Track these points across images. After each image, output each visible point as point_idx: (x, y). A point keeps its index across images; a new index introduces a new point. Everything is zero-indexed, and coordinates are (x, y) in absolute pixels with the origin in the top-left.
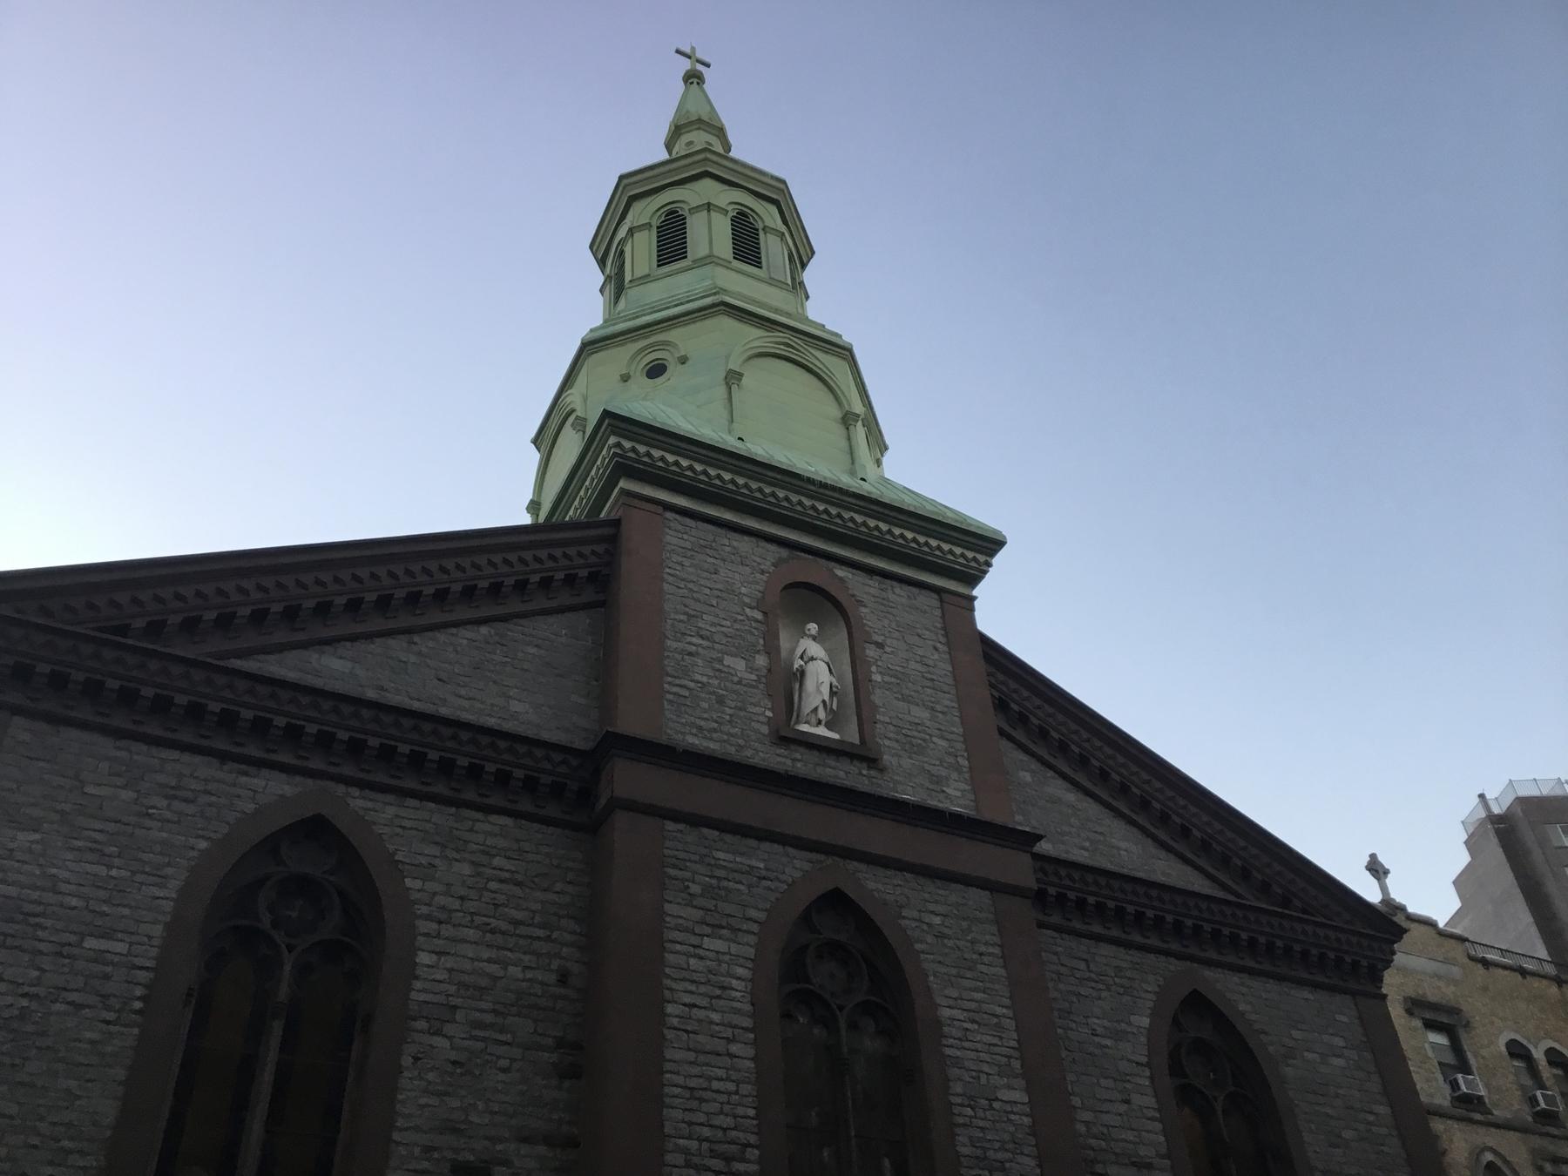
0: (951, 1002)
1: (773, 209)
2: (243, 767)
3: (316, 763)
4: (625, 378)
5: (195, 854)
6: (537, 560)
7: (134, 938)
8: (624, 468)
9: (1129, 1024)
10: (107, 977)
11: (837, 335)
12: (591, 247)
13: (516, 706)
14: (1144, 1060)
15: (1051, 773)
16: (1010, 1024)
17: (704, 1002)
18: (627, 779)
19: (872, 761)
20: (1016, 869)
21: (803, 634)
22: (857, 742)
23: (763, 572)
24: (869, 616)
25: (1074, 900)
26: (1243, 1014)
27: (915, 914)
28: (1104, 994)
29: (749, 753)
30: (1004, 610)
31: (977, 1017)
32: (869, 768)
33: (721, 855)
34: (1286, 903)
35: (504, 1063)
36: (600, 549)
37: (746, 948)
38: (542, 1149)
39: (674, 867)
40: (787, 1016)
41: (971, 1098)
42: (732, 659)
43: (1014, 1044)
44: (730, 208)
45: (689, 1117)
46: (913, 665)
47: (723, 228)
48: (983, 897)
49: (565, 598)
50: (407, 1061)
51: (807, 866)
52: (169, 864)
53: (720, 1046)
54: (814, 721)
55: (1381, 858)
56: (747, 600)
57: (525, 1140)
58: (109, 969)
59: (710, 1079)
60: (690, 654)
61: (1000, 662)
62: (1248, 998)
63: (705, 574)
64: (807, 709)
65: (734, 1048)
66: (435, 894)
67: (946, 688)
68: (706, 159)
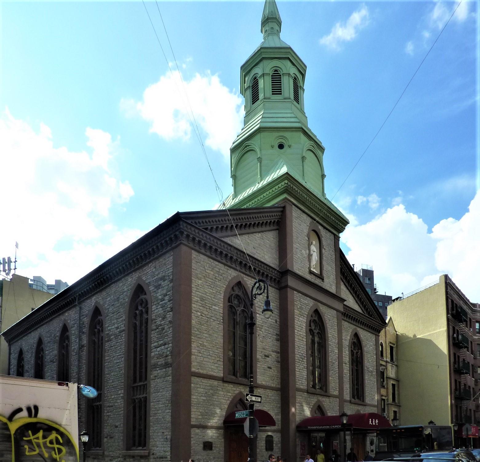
8: (286, 190)
10: (217, 314)
11: (320, 142)
16: (337, 338)
19: (323, 280)
32: (322, 281)
33: (302, 300)
38: (275, 353)
48: (335, 312)
50: (257, 336)
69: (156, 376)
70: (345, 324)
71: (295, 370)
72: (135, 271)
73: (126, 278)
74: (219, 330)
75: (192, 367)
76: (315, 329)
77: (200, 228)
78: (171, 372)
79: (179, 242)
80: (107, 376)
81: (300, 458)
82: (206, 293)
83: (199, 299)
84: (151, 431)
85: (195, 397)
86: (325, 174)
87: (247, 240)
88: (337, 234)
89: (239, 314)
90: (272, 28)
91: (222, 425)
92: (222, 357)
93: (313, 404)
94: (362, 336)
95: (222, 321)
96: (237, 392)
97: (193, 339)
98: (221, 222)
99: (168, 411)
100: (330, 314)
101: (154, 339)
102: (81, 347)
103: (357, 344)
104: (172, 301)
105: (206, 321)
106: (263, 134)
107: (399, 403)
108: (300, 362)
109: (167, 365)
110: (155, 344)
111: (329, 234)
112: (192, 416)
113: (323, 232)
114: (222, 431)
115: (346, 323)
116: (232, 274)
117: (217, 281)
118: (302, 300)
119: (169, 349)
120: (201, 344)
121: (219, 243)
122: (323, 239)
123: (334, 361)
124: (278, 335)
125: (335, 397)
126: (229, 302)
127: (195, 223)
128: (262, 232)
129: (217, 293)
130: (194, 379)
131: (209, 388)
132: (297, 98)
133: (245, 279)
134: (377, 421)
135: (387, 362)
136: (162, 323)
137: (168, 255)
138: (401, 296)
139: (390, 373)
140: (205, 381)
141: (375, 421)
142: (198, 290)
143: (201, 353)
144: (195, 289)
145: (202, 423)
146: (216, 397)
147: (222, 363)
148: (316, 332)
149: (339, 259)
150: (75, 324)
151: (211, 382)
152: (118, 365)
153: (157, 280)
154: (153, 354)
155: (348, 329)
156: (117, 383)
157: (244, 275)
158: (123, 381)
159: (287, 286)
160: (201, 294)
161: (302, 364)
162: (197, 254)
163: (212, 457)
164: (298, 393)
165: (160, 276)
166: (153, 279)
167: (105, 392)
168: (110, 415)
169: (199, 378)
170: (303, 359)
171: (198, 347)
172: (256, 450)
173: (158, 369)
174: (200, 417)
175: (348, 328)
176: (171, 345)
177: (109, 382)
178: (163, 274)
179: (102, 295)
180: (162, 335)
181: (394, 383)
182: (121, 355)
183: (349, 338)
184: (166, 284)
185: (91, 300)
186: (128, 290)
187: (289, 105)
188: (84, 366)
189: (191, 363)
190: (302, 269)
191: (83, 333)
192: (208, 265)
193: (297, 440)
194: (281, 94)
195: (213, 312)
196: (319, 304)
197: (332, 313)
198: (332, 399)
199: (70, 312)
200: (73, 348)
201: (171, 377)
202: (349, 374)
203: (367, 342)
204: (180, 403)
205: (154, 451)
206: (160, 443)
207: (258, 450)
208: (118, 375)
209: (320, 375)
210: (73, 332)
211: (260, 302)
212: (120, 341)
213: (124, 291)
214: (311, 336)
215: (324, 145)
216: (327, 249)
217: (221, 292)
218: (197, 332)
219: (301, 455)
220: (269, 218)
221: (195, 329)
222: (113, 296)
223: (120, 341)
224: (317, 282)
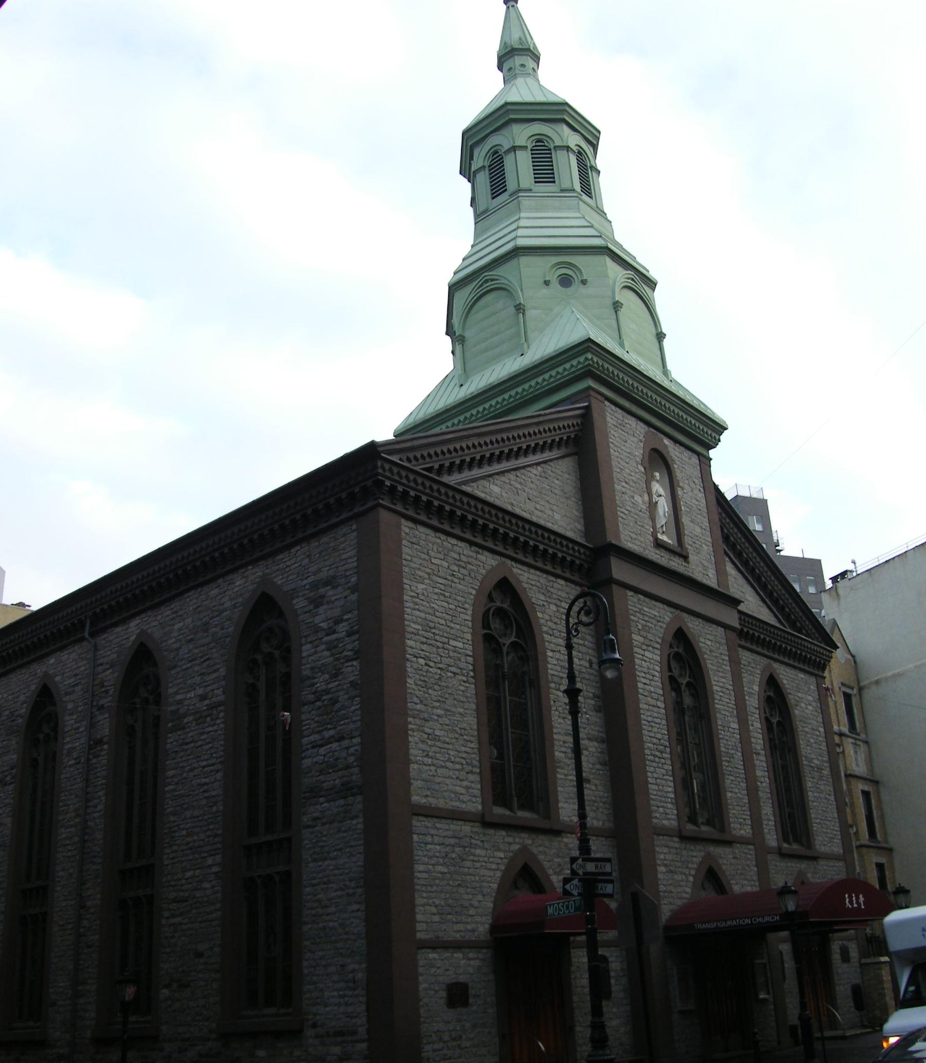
11: (644, 268)
16: (732, 693)
19: (685, 558)
29: (647, 552)
33: (645, 609)
38: (595, 744)
48: (721, 630)
50: (552, 703)
69: (317, 818)
70: (746, 657)
71: (647, 783)
72: (254, 562)
73: (230, 577)
74: (467, 697)
75: (412, 792)
76: (681, 675)
77: (417, 468)
78: (360, 806)
79: (370, 504)
80: (172, 818)
82: (435, 610)
83: (419, 627)
84: (305, 964)
85: (421, 868)
86: (664, 331)
87: (512, 482)
88: (704, 453)
89: (508, 653)
92: (477, 763)
93: (695, 866)
94: (785, 682)
95: (472, 674)
96: (516, 847)
97: (410, 723)
98: (460, 453)
99: (355, 907)
100: (711, 638)
101: (308, 724)
102: (95, 744)
103: (776, 699)
104: (357, 636)
105: (438, 677)
107: (886, 842)
108: (657, 759)
109: (347, 790)
110: (312, 738)
111: (687, 454)
112: (419, 917)
113: (674, 452)
115: (747, 654)
116: (486, 563)
117: (457, 581)
118: (645, 609)
119: (352, 750)
120: (428, 734)
121: (458, 497)
123: (732, 752)
124: (598, 697)
125: (744, 841)
126: (484, 627)
127: (409, 460)
128: (545, 462)
129: (459, 609)
130: (418, 824)
131: (452, 841)
132: (587, 187)
133: (515, 570)
135: (841, 735)
136: (329, 686)
137: (344, 529)
138: (851, 567)
139: (854, 765)
140: (442, 825)
141: (857, 898)
142: (417, 607)
143: (431, 757)
144: (411, 605)
145: (441, 934)
146: (467, 864)
147: (477, 778)
148: (684, 681)
149: (715, 509)
150: (77, 685)
151: (455, 826)
152: (204, 792)
153: (314, 586)
154: (307, 763)
155: (754, 668)
156: (202, 836)
157: (513, 563)
158: (220, 832)
159: (611, 581)
160: (423, 615)
162: (410, 524)
163: (468, 1025)
164: (659, 840)
165: (323, 575)
166: (305, 582)
167: (166, 863)
168: (181, 924)
169: (429, 819)
170: (662, 752)
171: (423, 742)
173: (322, 800)
174: (436, 918)
175: (752, 665)
176: (357, 740)
177: (177, 834)
178: (331, 573)
179: (159, 617)
180: (331, 716)
181: (866, 788)
182: (213, 765)
183: (756, 688)
184: (340, 596)
185: (126, 626)
186: (235, 606)
187: (574, 202)
188: (101, 793)
189: (410, 784)
190: (639, 538)
191: (101, 708)
192: (435, 547)
195: (451, 654)
196: (685, 615)
197: (714, 633)
198: (738, 849)
199: (64, 656)
200: (67, 747)
201: (361, 820)
202: (767, 779)
203: (799, 695)
204: (383, 884)
205: (318, 1017)
206: (335, 993)
207: (575, 998)
208: (206, 817)
209: (702, 787)
210: (70, 706)
212: (210, 729)
213: (221, 607)
214: (673, 694)
215: (653, 274)
216: (686, 486)
217: (467, 606)
218: (418, 707)
220: (558, 432)
221: (416, 700)
222: (190, 620)
223: (210, 729)
224: (673, 564)
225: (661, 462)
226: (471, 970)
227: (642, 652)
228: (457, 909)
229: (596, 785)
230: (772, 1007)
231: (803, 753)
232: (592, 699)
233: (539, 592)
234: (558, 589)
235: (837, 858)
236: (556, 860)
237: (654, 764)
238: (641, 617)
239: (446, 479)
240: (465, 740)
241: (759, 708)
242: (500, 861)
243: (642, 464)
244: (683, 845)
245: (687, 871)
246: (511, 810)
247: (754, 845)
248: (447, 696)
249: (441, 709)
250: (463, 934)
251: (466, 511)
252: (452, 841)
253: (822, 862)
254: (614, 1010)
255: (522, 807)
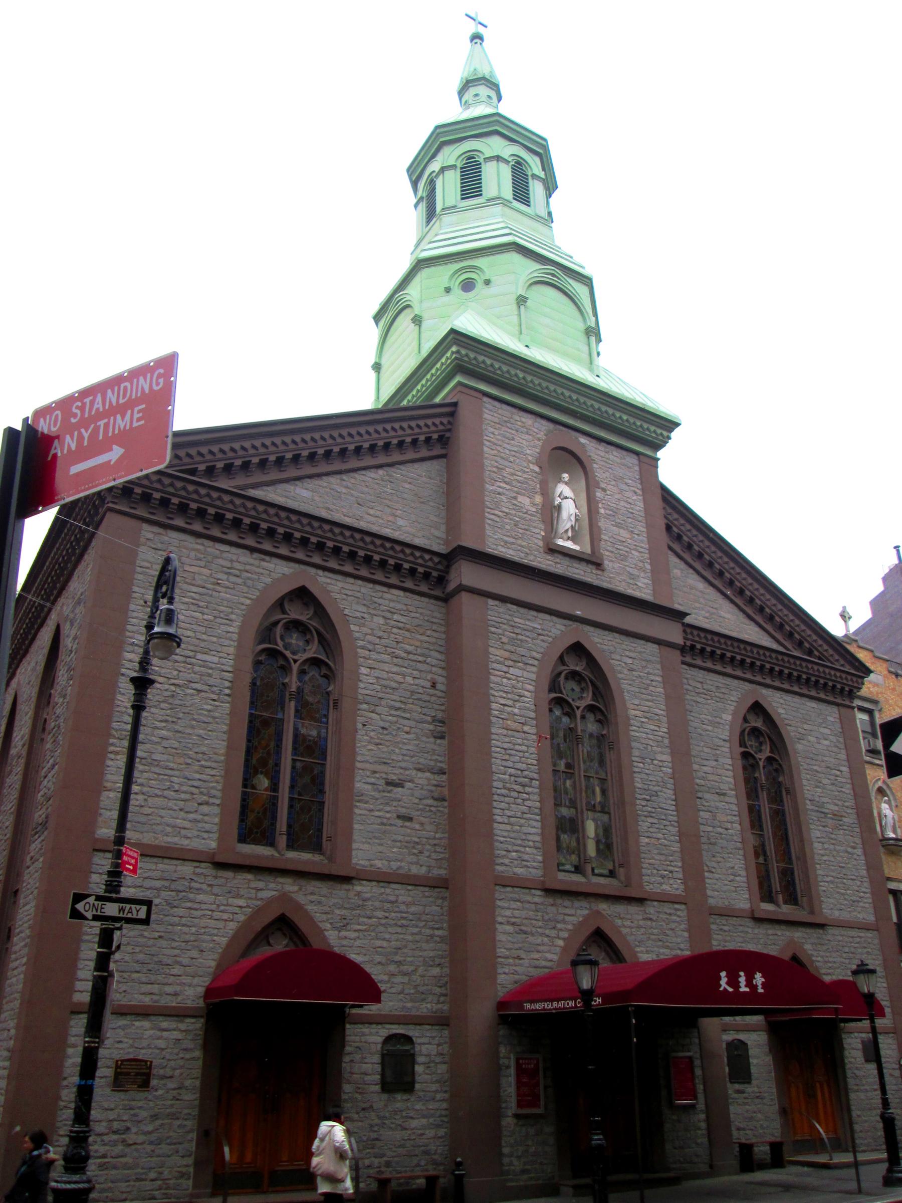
0: (636, 707)
1: (537, 160)
2: (263, 556)
3: (300, 555)
4: (448, 290)
5: (244, 607)
6: (410, 427)
7: (221, 655)
8: (460, 368)
9: (721, 718)
10: (210, 675)
12: (408, 170)
13: (400, 522)
14: (727, 738)
15: (691, 571)
17: (510, 703)
18: (467, 574)
19: (598, 565)
20: (673, 633)
21: (560, 480)
22: (589, 551)
23: (539, 439)
24: (600, 473)
25: (705, 650)
26: (779, 714)
27: (618, 657)
28: (709, 702)
30: (675, 468)
31: (648, 715)
32: (597, 569)
33: (517, 620)
34: (810, 653)
35: (406, 729)
36: (445, 420)
37: (531, 674)
38: (428, 774)
39: (494, 626)
40: (551, 710)
41: (643, 758)
42: (532, 504)
43: (666, 730)
44: (510, 160)
45: (505, 763)
46: (622, 503)
47: (506, 172)
48: (652, 648)
49: (424, 453)
50: (359, 726)
51: (563, 628)
52: (232, 613)
53: (519, 727)
54: (566, 537)
55: (848, 609)
56: (530, 458)
57: (419, 770)
58: (210, 671)
59: (514, 744)
60: (499, 494)
61: (670, 501)
62: (783, 706)
63: (507, 441)
64: (561, 530)
65: (526, 728)
66: (366, 634)
67: (640, 519)
68: (497, 121)
74: (214, 718)
81: (517, 1116)
90: (477, 95)
91: (201, 1003)
94: (781, 711)
106: (424, 273)
108: (515, 794)
114: (196, 1025)
118: (517, 620)
122: (595, 466)
125: (665, 899)
134: (759, 979)
146: (180, 912)
161: (519, 801)
172: (339, 1088)
193: (503, 1050)
194: (481, 195)
197: (639, 649)
203: (806, 726)
207: (347, 1088)
211: (372, 635)
219: (520, 1105)
225: (574, 461)
226: (161, 1043)
227: (505, 669)
228: (150, 967)
229: (422, 824)
230: (703, 1116)
231: (808, 795)
232: (430, 724)
233: (358, 603)
234: (390, 600)
235: (866, 928)
236: (338, 912)
237: (507, 799)
238: (509, 629)
239: (224, 483)
240: (202, 766)
241: (730, 741)
242: (237, 910)
243: (537, 464)
244: (551, 900)
245: (553, 933)
246: (778, 905)
247: (685, 904)
248: (181, 715)
249: (168, 730)
250: (155, 998)
251: (763, 661)
252: (158, 884)
253: (831, 931)
254: (418, 1107)
255: (291, 846)
